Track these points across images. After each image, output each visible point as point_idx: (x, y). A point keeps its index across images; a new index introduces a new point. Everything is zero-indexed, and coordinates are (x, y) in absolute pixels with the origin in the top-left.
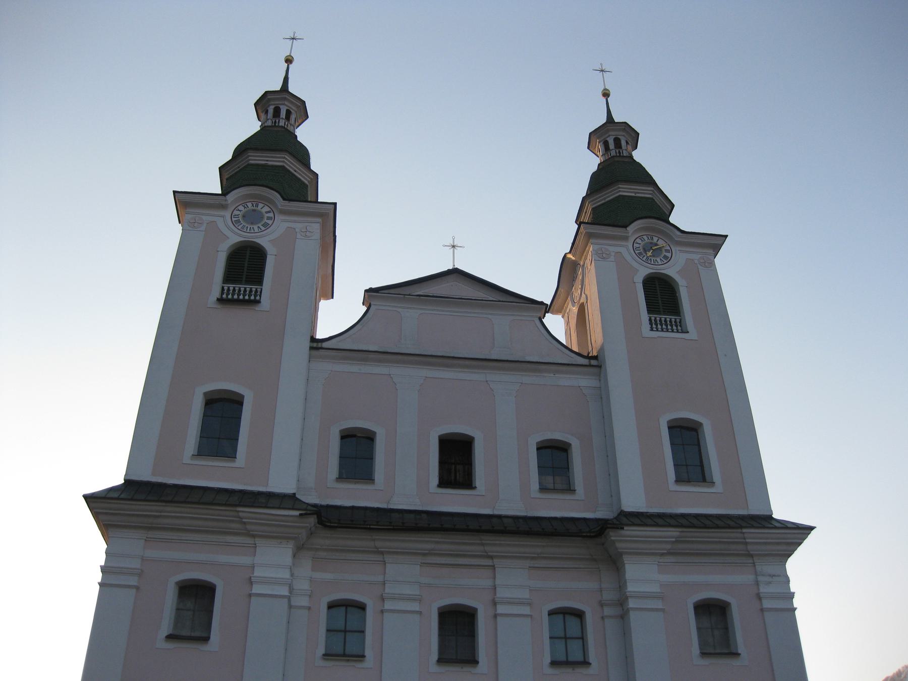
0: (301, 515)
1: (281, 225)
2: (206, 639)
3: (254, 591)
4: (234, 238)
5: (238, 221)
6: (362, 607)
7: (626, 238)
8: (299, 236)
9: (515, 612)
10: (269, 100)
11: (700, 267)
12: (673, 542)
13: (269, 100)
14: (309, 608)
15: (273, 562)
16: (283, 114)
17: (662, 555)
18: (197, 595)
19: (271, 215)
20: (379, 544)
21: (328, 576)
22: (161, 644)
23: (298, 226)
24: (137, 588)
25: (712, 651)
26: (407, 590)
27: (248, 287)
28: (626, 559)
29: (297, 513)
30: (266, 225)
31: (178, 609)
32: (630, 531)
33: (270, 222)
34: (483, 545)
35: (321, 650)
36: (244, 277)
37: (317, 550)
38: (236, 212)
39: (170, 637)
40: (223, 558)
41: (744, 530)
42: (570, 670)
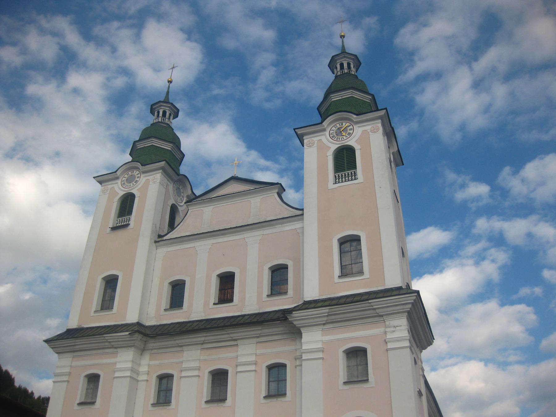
0: (129, 334)
1: (358, 130)
2: (367, 380)
3: (389, 347)
4: (334, 147)
5: (124, 183)
6: (284, 366)
7: (324, 130)
8: (370, 133)
9: (249, 369)
10: (155, 109)
11: (370, 133)
12: (327, 316)
13: (336, 60)
14: (147, 381)
15: (124, 359)
16: (345, 65)
17: (324, 324)
18: (357, 354)
19: (351, 127)
20: (178, 342)
21: (157, 362)
22: (341, 387)
23: (151, 178)
24: (68, 381)
25: (356, 380)
26: (193, 364)
27: (349, 172)
28: (301, 329)
29: (127, 333)
30: (136, 182)
31: (87, 389)
32: (296, 314)
33: (351, 132)
34: (228, 334)
35: (264, 394)
36: (346, 168)
37: (152, 350)
38: (124, 179)
39: (80, 404)
40: (104, 361)
41: (370, 301)
42: (275, 400)
